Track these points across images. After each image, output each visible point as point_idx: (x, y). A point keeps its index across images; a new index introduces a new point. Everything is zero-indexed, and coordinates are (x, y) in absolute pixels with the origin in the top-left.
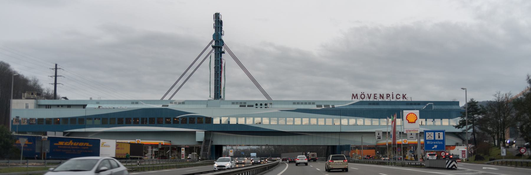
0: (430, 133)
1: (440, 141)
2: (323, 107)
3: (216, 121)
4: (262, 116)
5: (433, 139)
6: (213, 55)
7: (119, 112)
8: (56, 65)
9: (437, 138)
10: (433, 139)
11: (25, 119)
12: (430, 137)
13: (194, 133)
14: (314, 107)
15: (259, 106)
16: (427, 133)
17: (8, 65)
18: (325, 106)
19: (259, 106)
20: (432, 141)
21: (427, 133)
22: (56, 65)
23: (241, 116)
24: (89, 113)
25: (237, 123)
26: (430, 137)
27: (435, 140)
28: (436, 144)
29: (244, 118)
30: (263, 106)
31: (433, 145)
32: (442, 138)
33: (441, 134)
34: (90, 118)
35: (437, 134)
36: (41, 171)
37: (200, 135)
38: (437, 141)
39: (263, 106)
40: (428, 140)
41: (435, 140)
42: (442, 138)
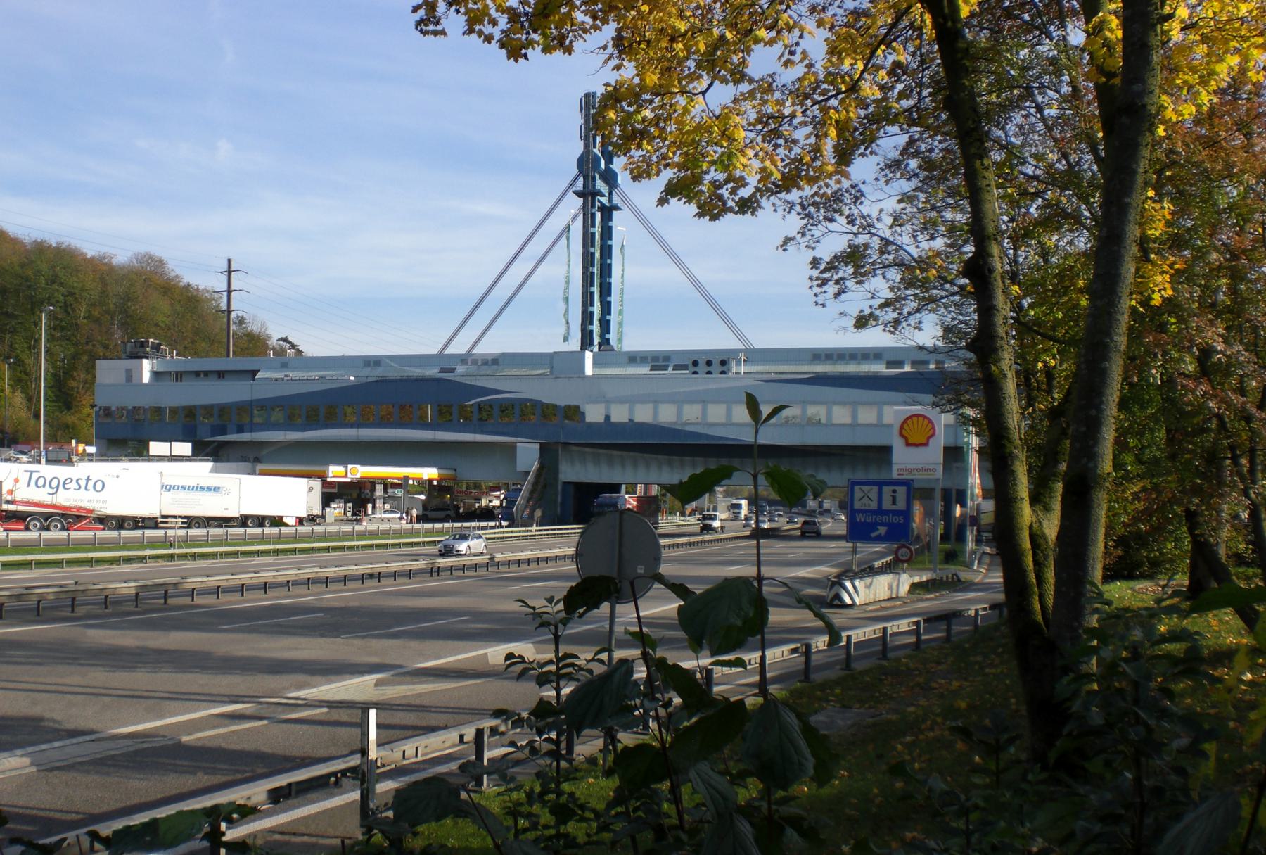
0: (866, 488)
1: (896, 513)
2: (907, 368)
3: (594, 414)
4: (703, 400)
5: (874, 505)
6: (578, 226)
7: (321, 391)
8: (229, 261)
9: (887, 505)
10: (874, 505)
11: (123, 408)
12: (865, 500)
13: (512, 448)
14: (879, 368)
15: (702, 368)
16: (857, 488)
17: (161, 262)
18: (914, 363)
19: (702, 368)
20: (873, 512)
21: (857, 488)
22: (229, 261)
23: (643, 400)
24: (261, 393)
25: (631, 420)
26: (865, 500)
27: (880, 511)
28: (882, 524)
29: (627, 406)
30: (716, 367)
31: (874, 526)
32: (901, 505)
33: (901, 491)
34: (266, 405)
35: (887, 490)
36: (724, 462)
37: (528, 454)
38: (887, 512)
39: (716, 367)
40: (860, 511)
41: (880, 511)
42: (901, 505)
